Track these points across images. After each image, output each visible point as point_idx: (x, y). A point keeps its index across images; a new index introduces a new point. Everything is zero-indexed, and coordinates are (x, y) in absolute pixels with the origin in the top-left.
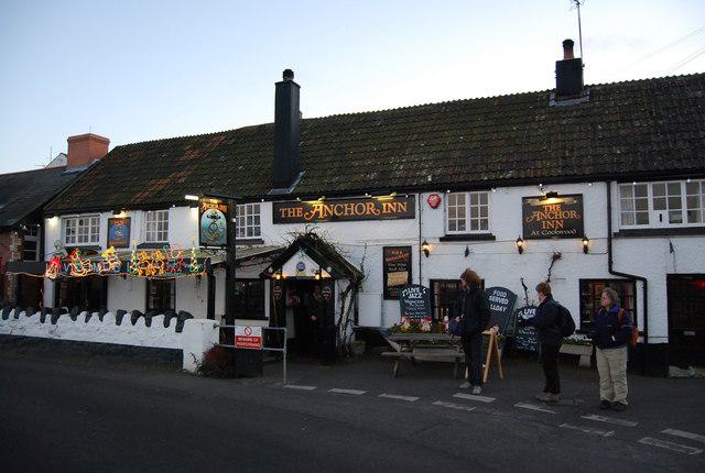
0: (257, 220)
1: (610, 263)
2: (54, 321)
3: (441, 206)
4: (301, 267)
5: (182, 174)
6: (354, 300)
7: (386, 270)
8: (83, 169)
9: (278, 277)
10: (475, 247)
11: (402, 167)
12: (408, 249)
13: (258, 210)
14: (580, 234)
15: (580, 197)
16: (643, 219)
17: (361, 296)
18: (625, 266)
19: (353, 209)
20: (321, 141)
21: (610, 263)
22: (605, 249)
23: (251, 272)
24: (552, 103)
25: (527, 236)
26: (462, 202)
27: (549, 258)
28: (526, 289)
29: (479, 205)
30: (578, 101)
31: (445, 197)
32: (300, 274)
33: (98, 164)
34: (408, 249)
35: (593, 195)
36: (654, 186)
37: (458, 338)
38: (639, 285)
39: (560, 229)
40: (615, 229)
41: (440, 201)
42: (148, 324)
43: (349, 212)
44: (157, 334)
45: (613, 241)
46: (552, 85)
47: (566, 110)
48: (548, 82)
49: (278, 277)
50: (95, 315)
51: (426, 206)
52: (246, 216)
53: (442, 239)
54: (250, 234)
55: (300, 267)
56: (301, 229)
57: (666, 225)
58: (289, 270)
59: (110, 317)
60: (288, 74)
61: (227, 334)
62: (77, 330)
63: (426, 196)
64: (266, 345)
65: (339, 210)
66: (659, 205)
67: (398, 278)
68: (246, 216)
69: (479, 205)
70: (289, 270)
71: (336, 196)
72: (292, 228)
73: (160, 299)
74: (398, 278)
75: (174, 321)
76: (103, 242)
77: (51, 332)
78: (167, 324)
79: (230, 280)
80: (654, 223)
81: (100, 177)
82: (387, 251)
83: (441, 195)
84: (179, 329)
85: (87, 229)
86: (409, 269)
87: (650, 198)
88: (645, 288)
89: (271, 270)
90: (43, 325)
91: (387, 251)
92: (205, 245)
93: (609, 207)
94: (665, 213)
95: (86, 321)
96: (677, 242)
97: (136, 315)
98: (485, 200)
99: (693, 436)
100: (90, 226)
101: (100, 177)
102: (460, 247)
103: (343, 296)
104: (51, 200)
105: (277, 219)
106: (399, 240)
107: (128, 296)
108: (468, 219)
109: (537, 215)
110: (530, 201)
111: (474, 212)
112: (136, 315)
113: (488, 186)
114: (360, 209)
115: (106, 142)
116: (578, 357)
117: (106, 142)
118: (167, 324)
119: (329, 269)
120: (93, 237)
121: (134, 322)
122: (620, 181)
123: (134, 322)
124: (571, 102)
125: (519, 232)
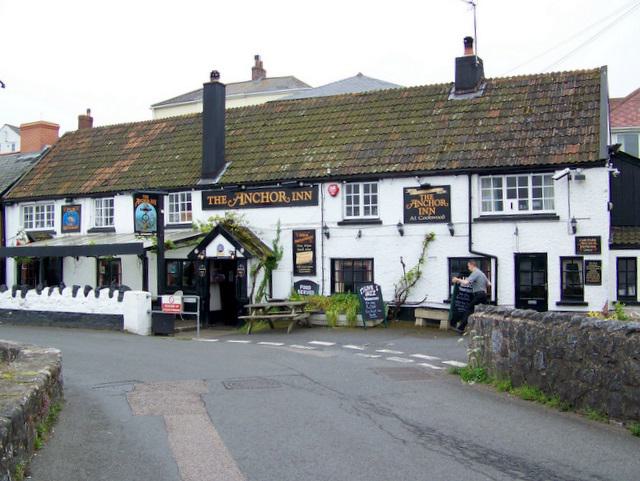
0: (189, 207)
1: (470, 243)
2: (23, 295)
3: (340, 195)
4: (221, 249)
5: (125, 163)
6: (269, 276)
7: (295, 251)
8: (35, 156)
9: (202, 257)
10: (367, 230)
11: (311, 158)
12: (312, 232)
13: (189, 198)
14: (448, 219)
15: (447, 188)
16: (500, 206)
17: (275, 273)
18: (482, 246)
19: (268, 197)
20: (249, 131)
21: (470, 243)
22: (468, 233)
23: (183, 253)
24: (451, 97)
25: (407, 220)
26: (357, 190)
27: (423, 239)
28: (404, 266)
29: (353, 206)
30: (472, 96)
31: (342, 188)
32: (220, 255)
33: (49, 151)
34: (312, 232)
35: (458, 186)
36: (534, 177)
37: (448, 307)
38: (493, 261)
39: (432, 215)
40: (475, 215)
41: (338, 190)
42: (97, 294)
43: (265, 199)
44: (104, 304)
45: (473, 226)
46: (452, 79)
47: (462, 104)
48: (448, 76)
49: (202, 257)
50: (56, 290)
51: (327, 195)
52: (180, 203)
53: (340, 224)
54: (183, 219)
55: (220, 248)
56: (221, 215)
57: (516, 211)
58: (211, 251)
59: (68, 291)
60: (215, 75)
61: (157, 304)
62: (42, 302)
63: (327, 186)
64: (185, 310)
65: (257, 198)
66: (511, 195)
67: (304, 257)
68: (180, 203)
69: (353, 206)
70: (211, 251)
71: (254, 185)
72: (213, 214)
73: (109, 276)
74: (304, 257)
75: (116, 293)
76: (57, 227)
77: (21, 305)
78: (111, 296)
79: (163, 264)
80: (507, 211)
81: (53, 165)
82: (296, 234)
83: (339, 185)
84: (120, 299)
85: (43, 215)
86: (313, 249)
87: (505, 188)
88: (496, 262)
89: (196, 251)
90: (99, 299)
91: (296, 234)
92: (139, 232)
93: (470, 198)
94: (515, 202)
95: (49, 295)
96: (523, 226)
97: (88, 289)
98: (375, 189)
99: (428, 357)
100: (46, 212)
101: (53, 165)
102: (353, 231)
103: (254, 274)
104: (9, 188)
105: (206, 206)
106: (305, 224)
107: (81, 271)
108: (362, 205)
109: (415, 203)
110: (409, 191)
111: (366, 200)
112: (88, 289)
113: (377, 177)
114: (274, 197)
115: (56, 128)
116: (438, 322)
117: (56, 128)
118: (111, 296)
119: (242, 250)
120: (49, 223)
121: (86, 295)
122: (481, 174)
123: (86, 295)
124: (465, 97)
125: (400, 218)
